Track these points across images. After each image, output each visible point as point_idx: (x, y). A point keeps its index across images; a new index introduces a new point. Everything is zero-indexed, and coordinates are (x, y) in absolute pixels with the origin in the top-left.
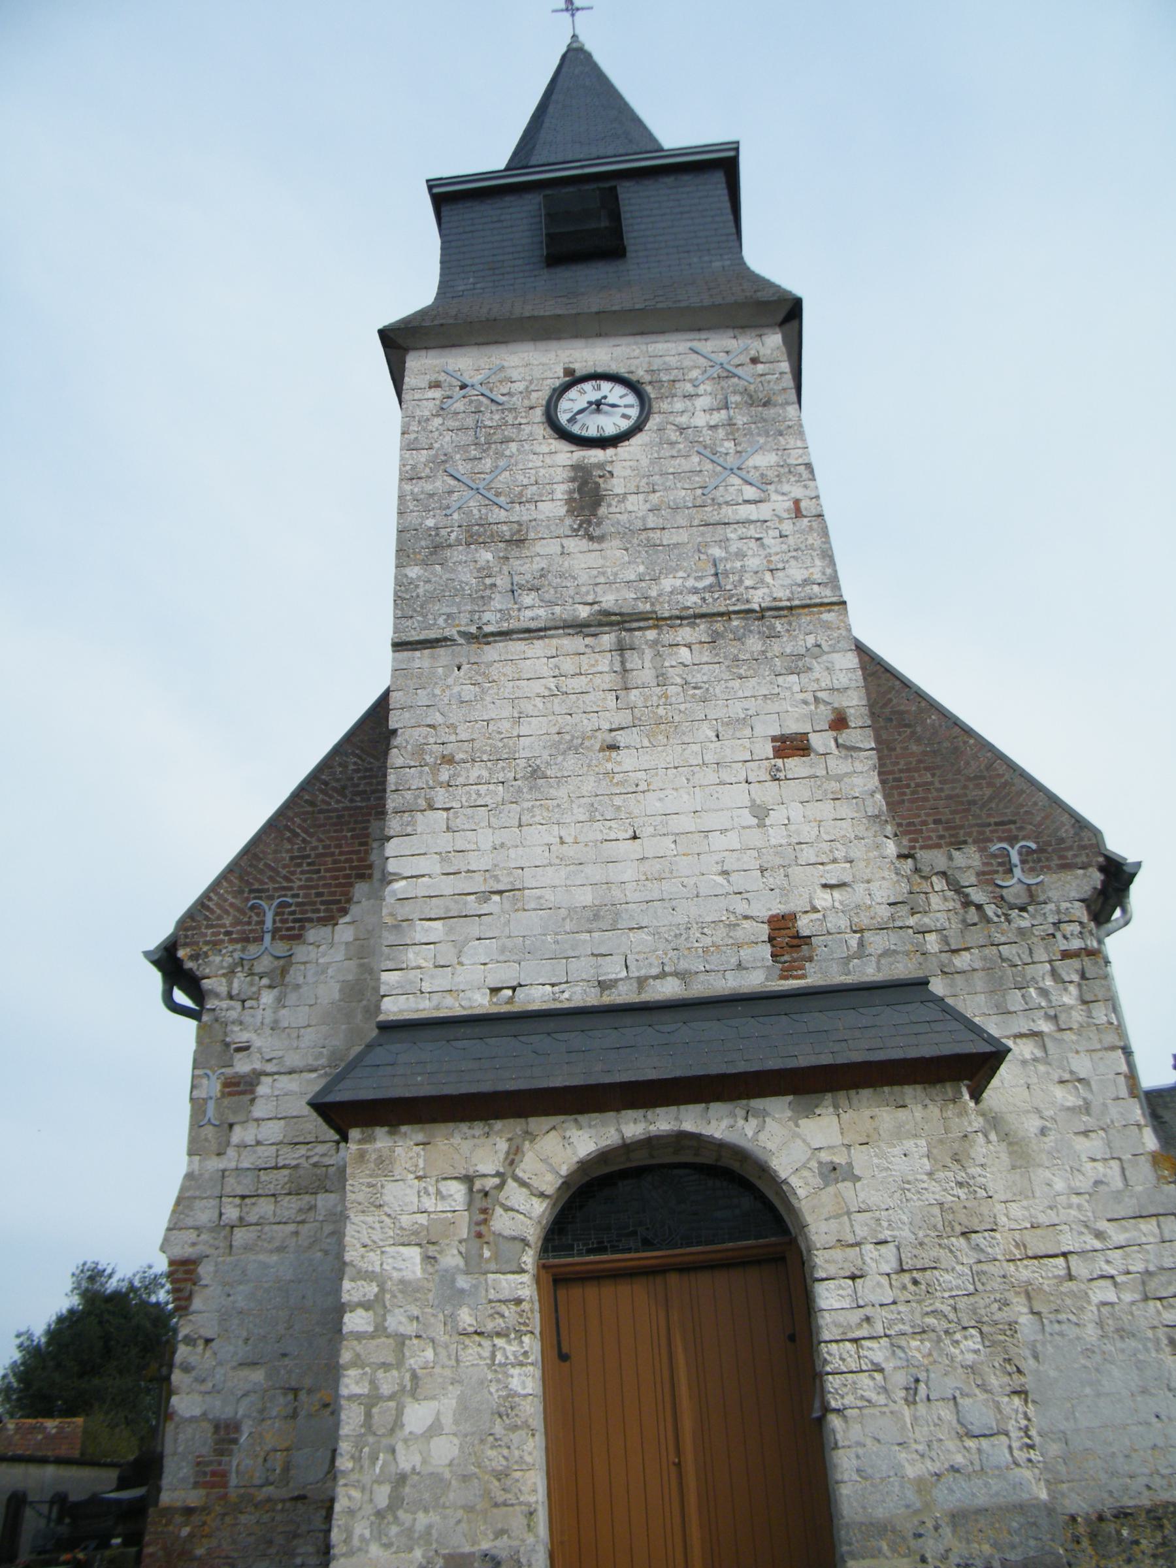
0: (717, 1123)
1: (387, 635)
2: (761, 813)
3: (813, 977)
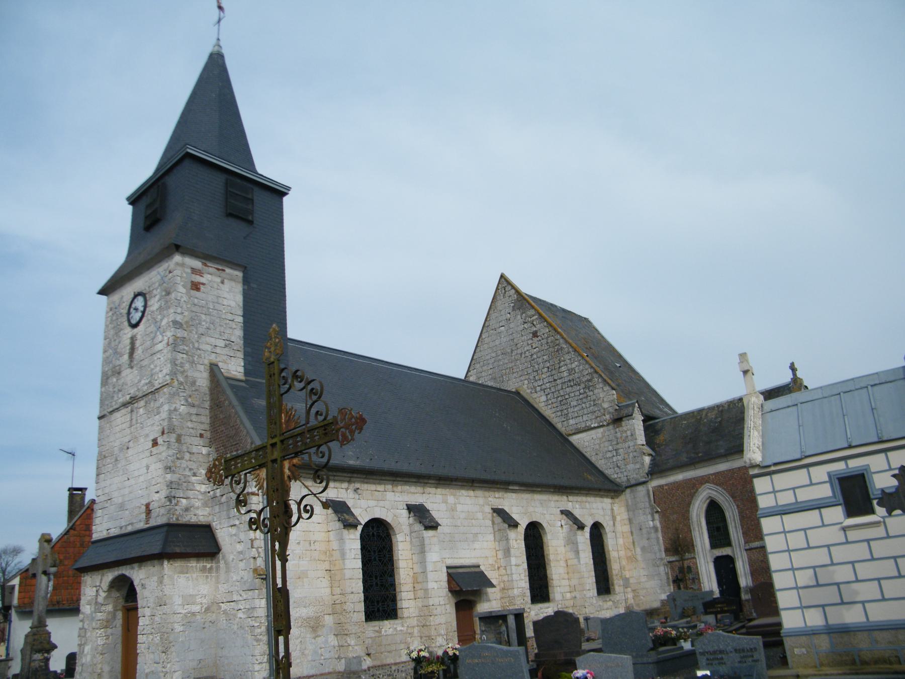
2: (148, 467)
3: (153, 523)
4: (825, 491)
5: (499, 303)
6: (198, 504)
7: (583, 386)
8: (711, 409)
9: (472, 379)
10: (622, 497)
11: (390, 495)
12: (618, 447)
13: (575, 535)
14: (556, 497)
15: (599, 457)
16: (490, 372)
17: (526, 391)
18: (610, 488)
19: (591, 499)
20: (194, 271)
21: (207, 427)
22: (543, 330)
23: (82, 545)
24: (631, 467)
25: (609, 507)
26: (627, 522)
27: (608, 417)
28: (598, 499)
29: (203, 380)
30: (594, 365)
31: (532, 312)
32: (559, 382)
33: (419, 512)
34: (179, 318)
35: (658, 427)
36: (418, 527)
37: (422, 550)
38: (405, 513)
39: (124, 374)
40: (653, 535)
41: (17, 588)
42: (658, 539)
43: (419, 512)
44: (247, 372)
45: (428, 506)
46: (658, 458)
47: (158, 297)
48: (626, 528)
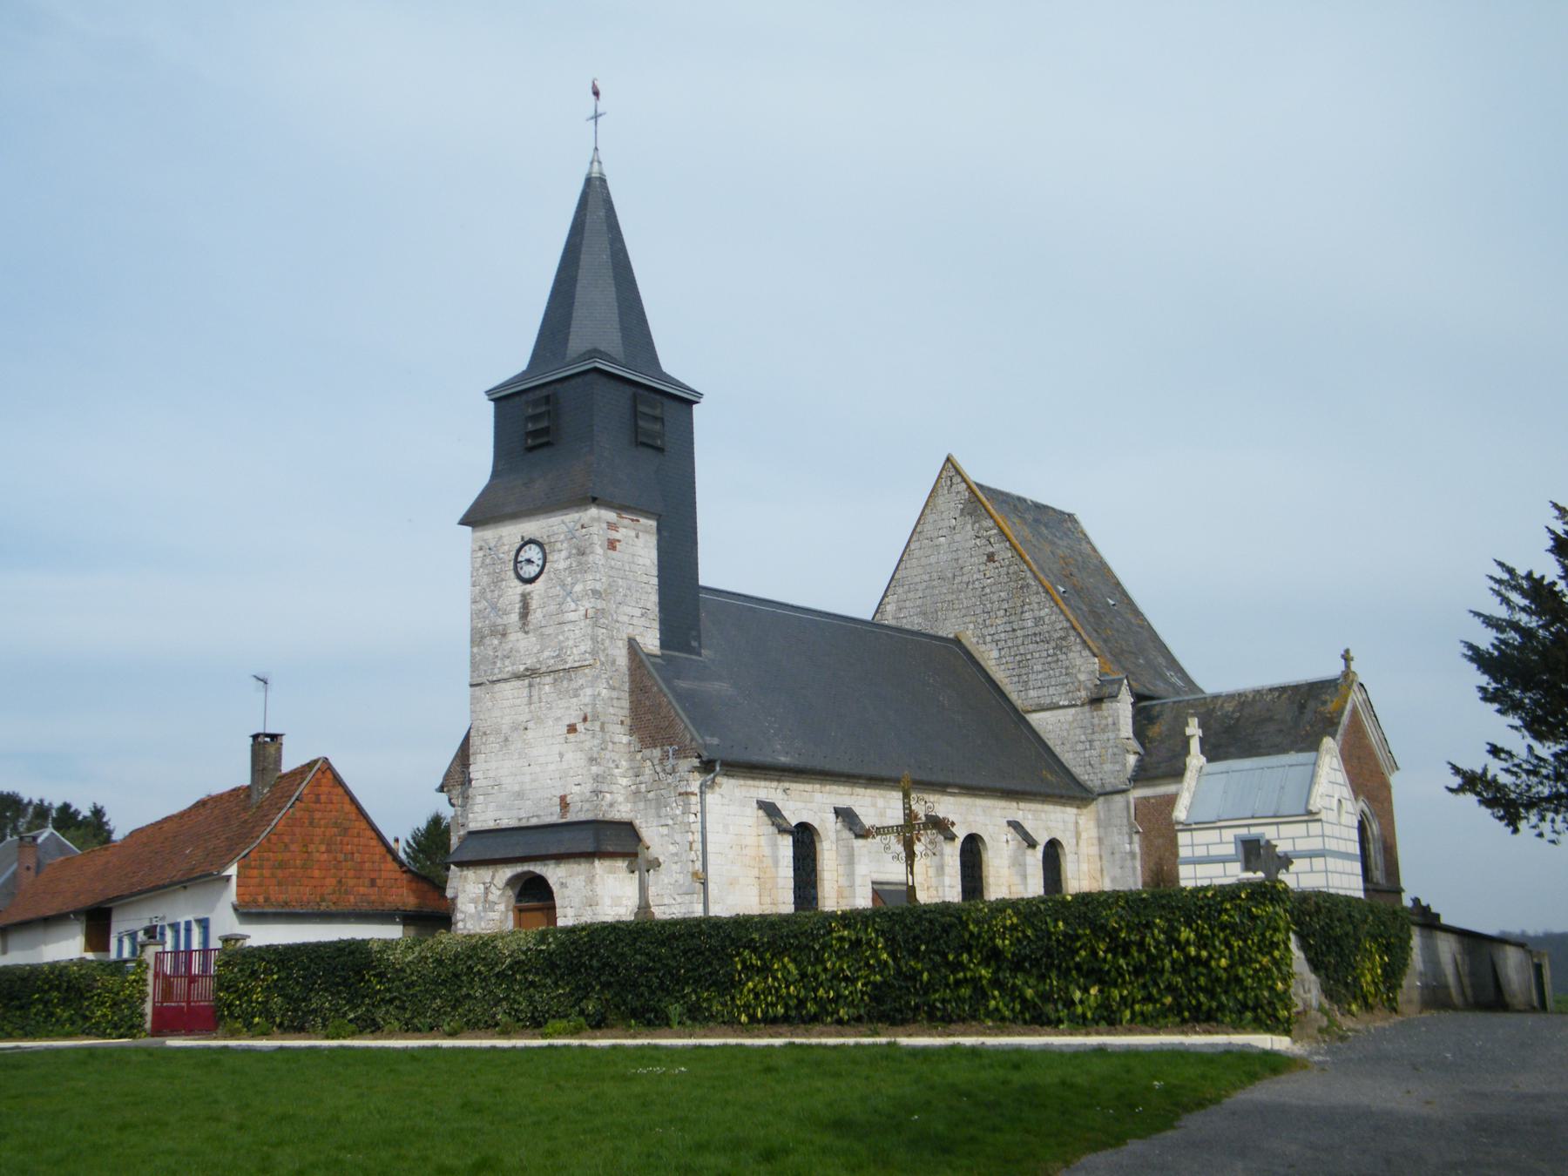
0: (537, 868)
1: (467, 680)
2: (561, 755)
3: (571, 817)
4: (1230, 849)
5: (940, 500)
6: (621, 799)
7: (1053, 644)
8: (1230, 697)
9: (889, 620)
10: (1093, 807)
11: (818, 796)
12: (1095, 737)
13: (1024, 854)
14: (1002, 804)
15: (1067, 747)
16: (919, 602)
17: (969, 639)
18: (1073, 792)
19: (1048, 808)
20: (612, 526)
21: (626, 712)
22: (999, 547)
23: (311, 824)
24: (1108, 767)
25: (1073, 819)
26: (1095, 842)
27: (1083, 694)
28: (1058, 808)
29: (622, 660)
30: (1071, 617)
31: (989, 523)
32: (1019, 633)
33: (846, 816)
34: (598, 586)
35: (1155, 712)
36: (847, 834)
37: (850, 860)
38: (832, 816)
39: (512, 637)
40: (1128, 863)
41: (234, 880)
42: (1134, 868)
43: (846, 816)
44: (663, 645)
45: (857, 810)
46: (1147, 759)
47: (564, 554)
48: (1094, 850)
